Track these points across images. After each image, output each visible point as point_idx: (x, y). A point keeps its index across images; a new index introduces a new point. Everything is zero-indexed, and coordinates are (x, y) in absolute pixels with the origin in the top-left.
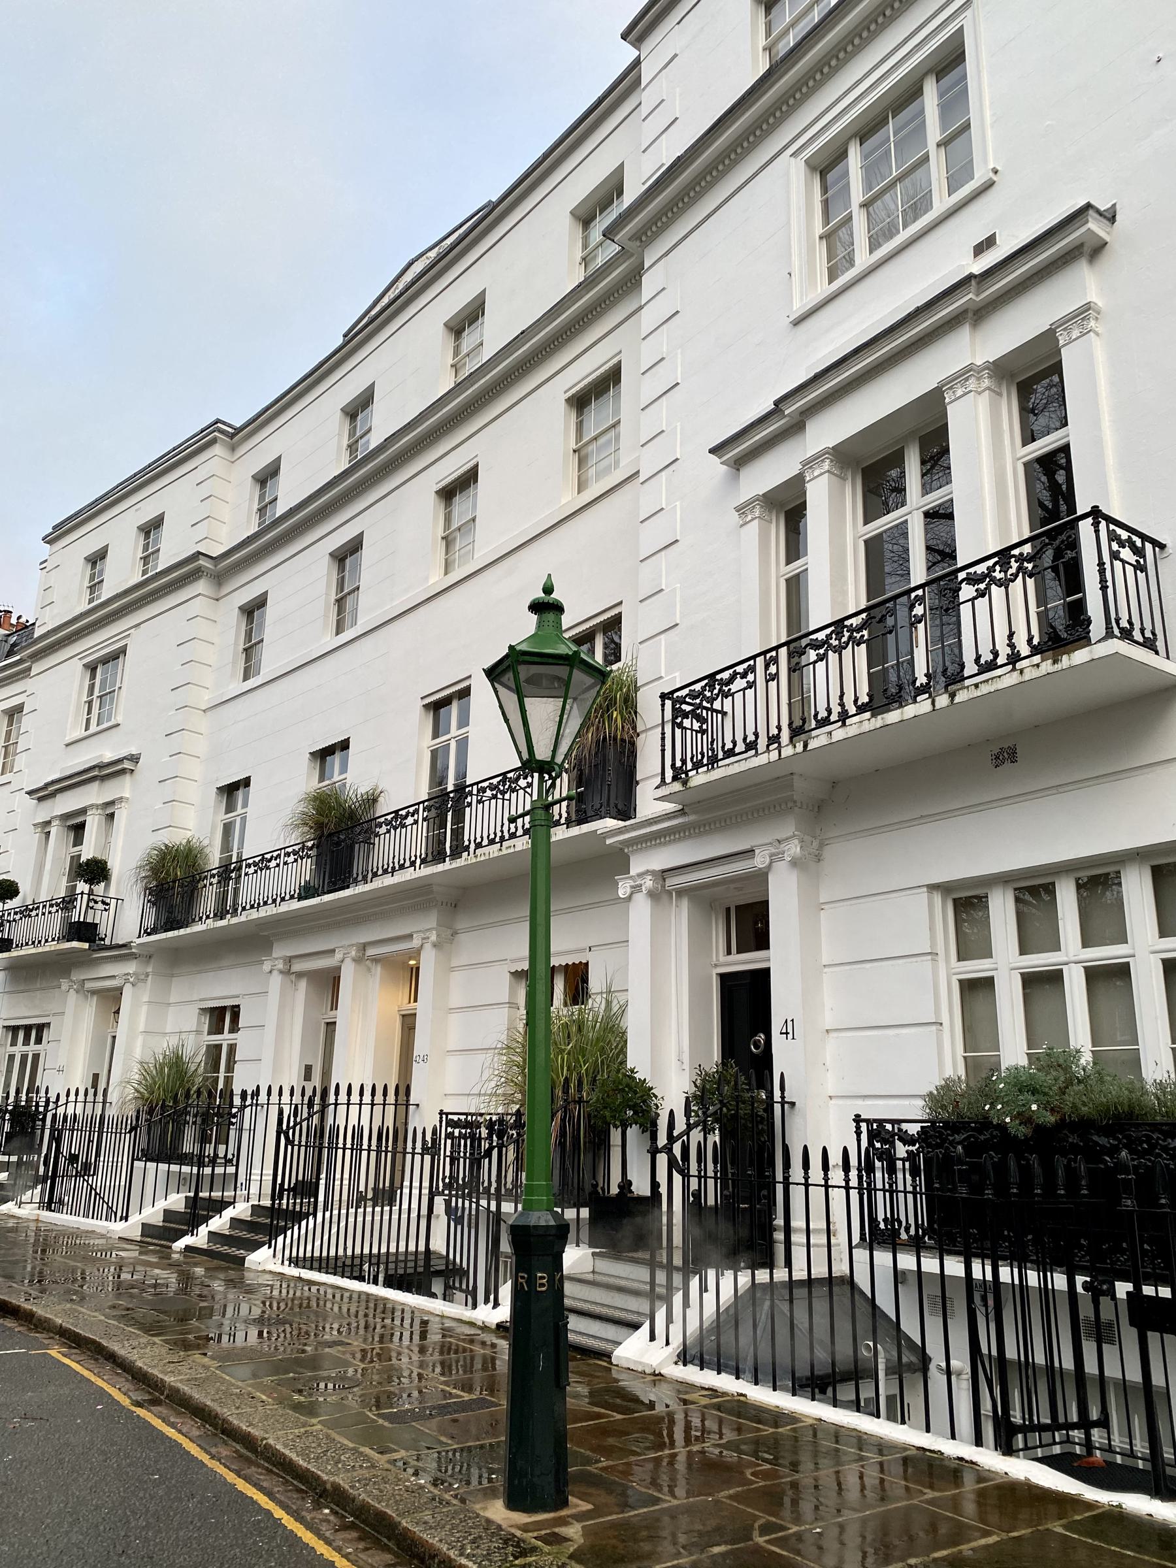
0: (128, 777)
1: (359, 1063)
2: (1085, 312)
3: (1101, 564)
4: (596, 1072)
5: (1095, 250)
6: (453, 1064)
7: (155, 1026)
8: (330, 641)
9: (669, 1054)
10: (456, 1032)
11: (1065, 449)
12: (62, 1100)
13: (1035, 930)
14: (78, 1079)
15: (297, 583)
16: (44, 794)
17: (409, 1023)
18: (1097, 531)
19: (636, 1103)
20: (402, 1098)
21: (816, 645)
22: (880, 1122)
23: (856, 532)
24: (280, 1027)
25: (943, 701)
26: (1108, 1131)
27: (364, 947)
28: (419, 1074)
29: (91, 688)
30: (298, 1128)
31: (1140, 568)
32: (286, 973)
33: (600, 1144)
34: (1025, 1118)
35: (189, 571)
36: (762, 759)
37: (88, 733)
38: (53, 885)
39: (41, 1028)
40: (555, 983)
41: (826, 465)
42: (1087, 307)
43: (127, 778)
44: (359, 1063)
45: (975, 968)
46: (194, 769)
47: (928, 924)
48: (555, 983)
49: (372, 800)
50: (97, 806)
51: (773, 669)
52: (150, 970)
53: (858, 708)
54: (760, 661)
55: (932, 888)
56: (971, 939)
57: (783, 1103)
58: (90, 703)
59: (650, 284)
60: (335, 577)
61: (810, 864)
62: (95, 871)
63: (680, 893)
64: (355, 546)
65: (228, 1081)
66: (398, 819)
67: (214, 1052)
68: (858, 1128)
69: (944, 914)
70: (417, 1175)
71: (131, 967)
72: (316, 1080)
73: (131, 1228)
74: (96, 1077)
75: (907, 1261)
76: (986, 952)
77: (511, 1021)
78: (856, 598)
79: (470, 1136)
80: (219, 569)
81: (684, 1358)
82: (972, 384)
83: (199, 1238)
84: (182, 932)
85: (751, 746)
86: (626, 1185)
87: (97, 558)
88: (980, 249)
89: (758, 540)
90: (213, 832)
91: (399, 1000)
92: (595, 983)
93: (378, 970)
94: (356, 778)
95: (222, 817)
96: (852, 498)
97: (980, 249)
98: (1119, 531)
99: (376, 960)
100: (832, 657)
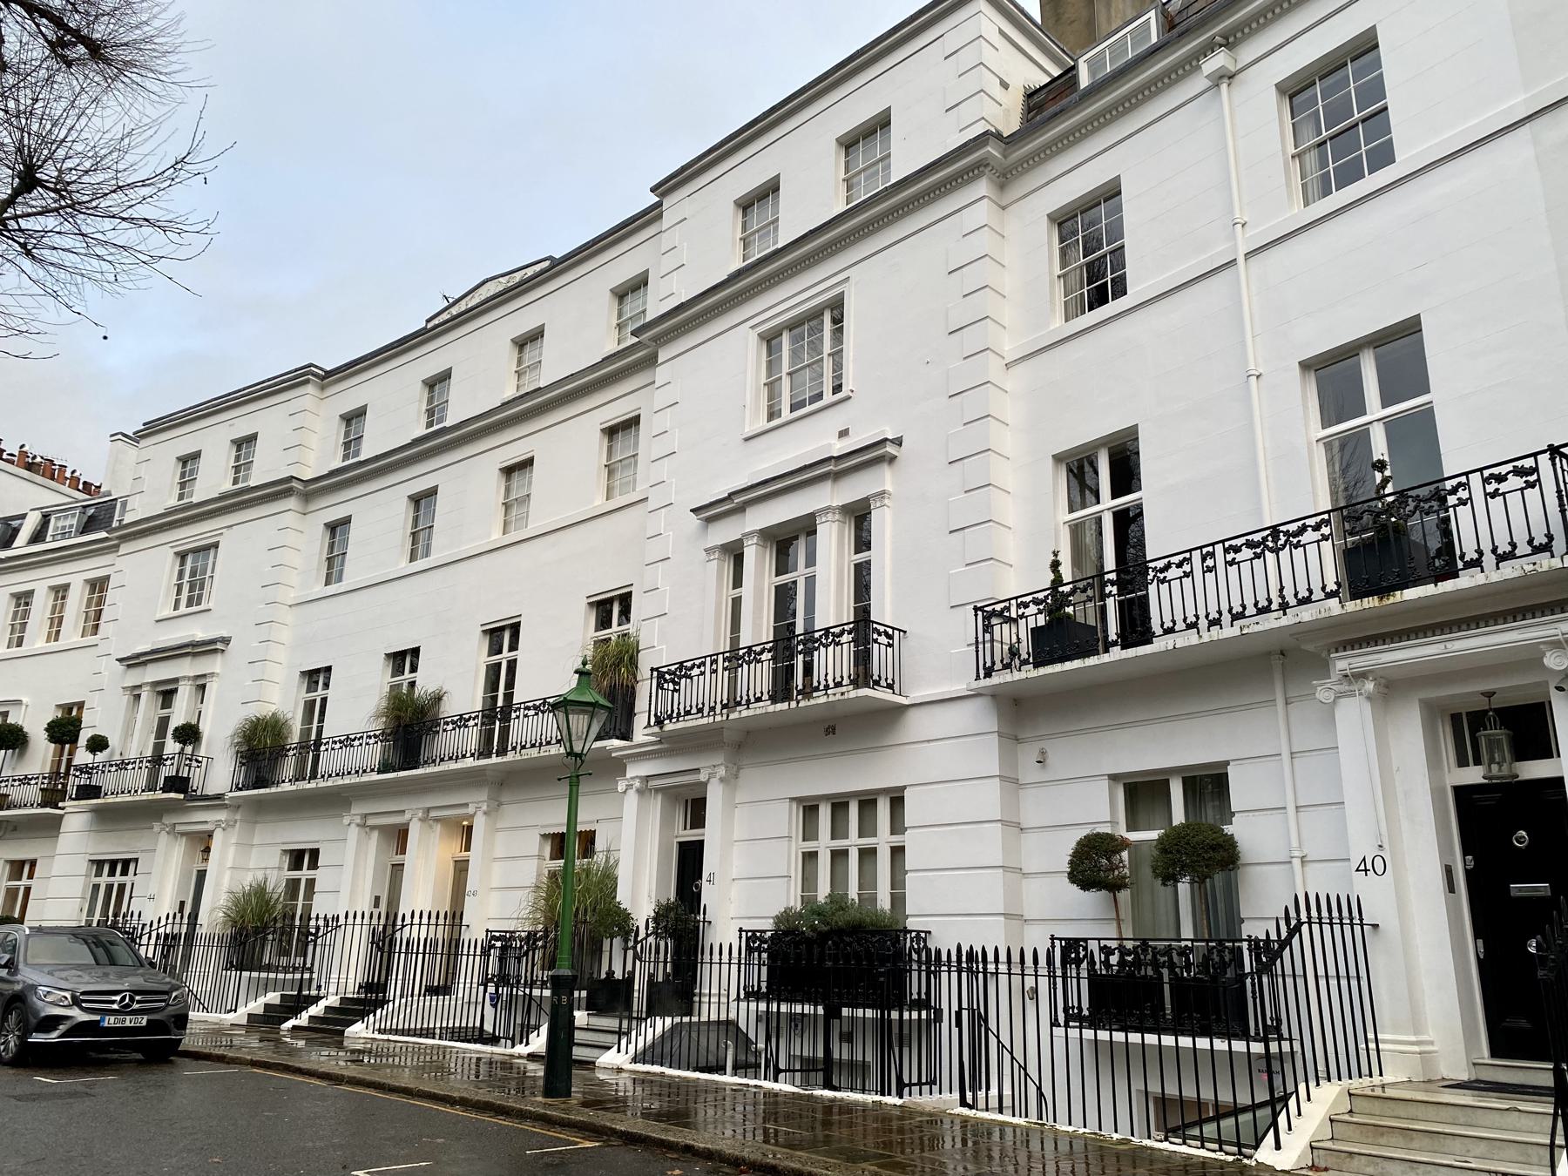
0: (219, 656)
1: (422, 893)
4: (597, 902)
6: (495, 897)
7: (242, 863)
8: (404, 566)
9: (641, 891)
10: (498, 874)
12: (163, 922)
13: (838, 831)
14: (167, 906)
15: (379, 515)
16: (134, 662)
17: (461, 868)
18: (1554, 465)
19: (620, 923)
20: (457, 921)
22: (754, 932)
23: (771, 581)
24: (356, 865)
25: (793, 704)
26: (850, 934)
27: (428, 810)
28: (469, 902)
29: (181, 574)
32: (363, 826)
33: (597, 951)
34: (813, 928)
35: (281, 489)
36: (705, 721)
37: (176, 613)
38: (140, 745)
39: (126, 863)
40: (570, 844)
42: (884, 492)
44: (422, 893)
45: (810, 846)
46: (280, 654)
47: (787, 819)
48: (570, 844)
49: (438, 699)
50: (189, 678)
51: (1210, 562)
52: (238, 817)
55: (792, 799)
56: (810, 832)
58: (180, 587)
59: (661, 374)
60: (411, 515)
62: (189, 734)
63: (657, 790)
65: (308, 909)
66: (461, 721)
67: (293, 885)
69: (797, 816)
70: (469, 969)
71: (222, 815)
72: (383, 908)
73: (240, 1016)
74: (182, 904)
77: (539, 868)
78: (767, 634)
79: (504, 946)
80: (311, 491)
81: (635, 1060)
82: (830, 516)
83: (303, 1019)
85: (700, 711)
86: (610, 973)
87: (189, 460)
88: (843, 434)
89: (716, 572)
91: (453, 849)
92: (600, 845)
93: (438, 827)
94: (426, 680)
95: (305, 696)
96: (770, 562)
97: (843, 434)
99: (437, 820)
100: (1270, 556)
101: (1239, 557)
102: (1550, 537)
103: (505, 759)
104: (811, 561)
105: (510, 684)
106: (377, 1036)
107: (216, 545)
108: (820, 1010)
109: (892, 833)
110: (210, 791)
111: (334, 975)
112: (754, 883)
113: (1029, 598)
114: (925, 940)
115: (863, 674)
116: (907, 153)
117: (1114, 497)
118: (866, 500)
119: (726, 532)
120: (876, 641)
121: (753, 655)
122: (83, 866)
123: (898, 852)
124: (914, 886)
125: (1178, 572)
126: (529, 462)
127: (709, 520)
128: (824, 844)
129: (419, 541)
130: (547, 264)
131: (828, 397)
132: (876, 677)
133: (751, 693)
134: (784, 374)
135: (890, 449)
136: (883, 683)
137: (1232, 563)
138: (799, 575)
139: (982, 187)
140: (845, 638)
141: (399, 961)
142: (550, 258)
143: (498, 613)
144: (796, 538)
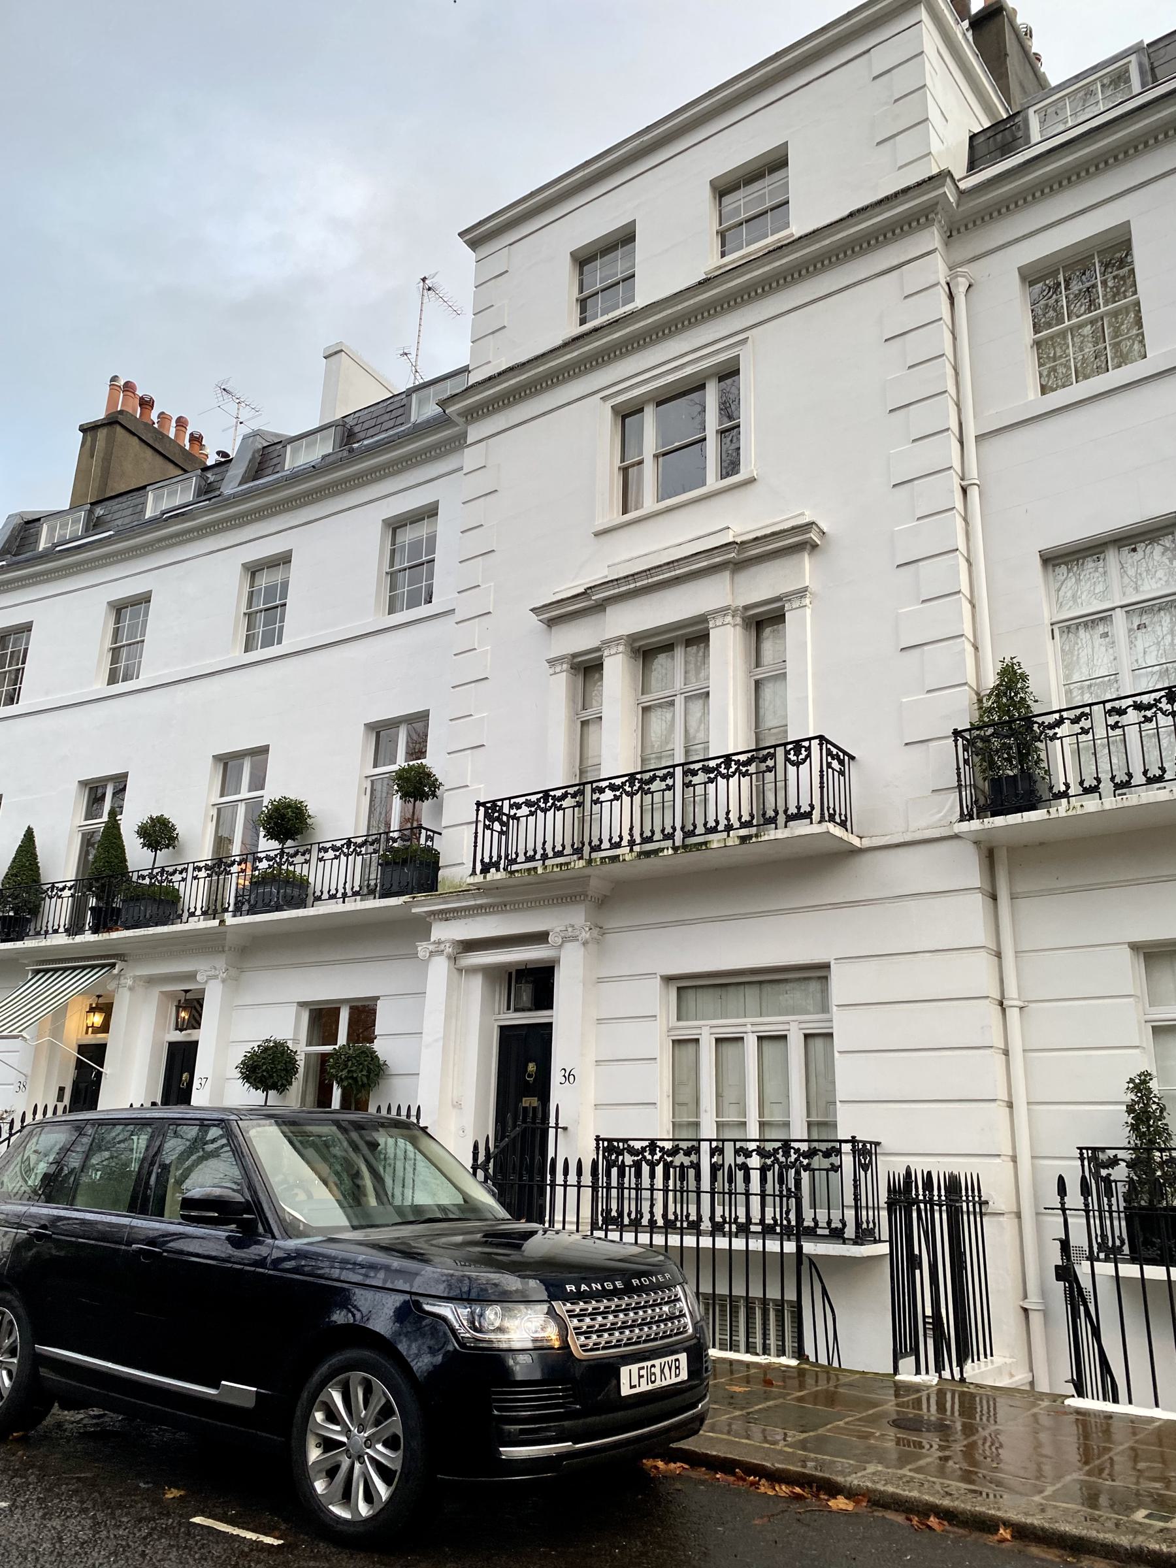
3: (821, 771)
21: (707, 770)
31: (842, 773)
41: (565, 666)
42: (805, 589)
47: (658, 1002)
53: (741, 823)
54: (506, 803)
57: (557, 1127)
59: (470, 457)
60: (111, 625)
61: (233, 982)
68: (1081, 1154)
75: (1130, 1270)
82: (729, 619)
84: (19, 945)
98: (832, 749)
101: (520, 813)
102: (812, 806)
103: (79, 939)
109: (679, 1019)
113: (329, 845)
116: (815, 201)
118: (703, 619)
119: (578, 638)
124: (849, 1077)
125: (663, 785)
129: (121, 663)
131: (713, 481)
135: (814, 536)
137: (321, 859)
139: (932, 238)
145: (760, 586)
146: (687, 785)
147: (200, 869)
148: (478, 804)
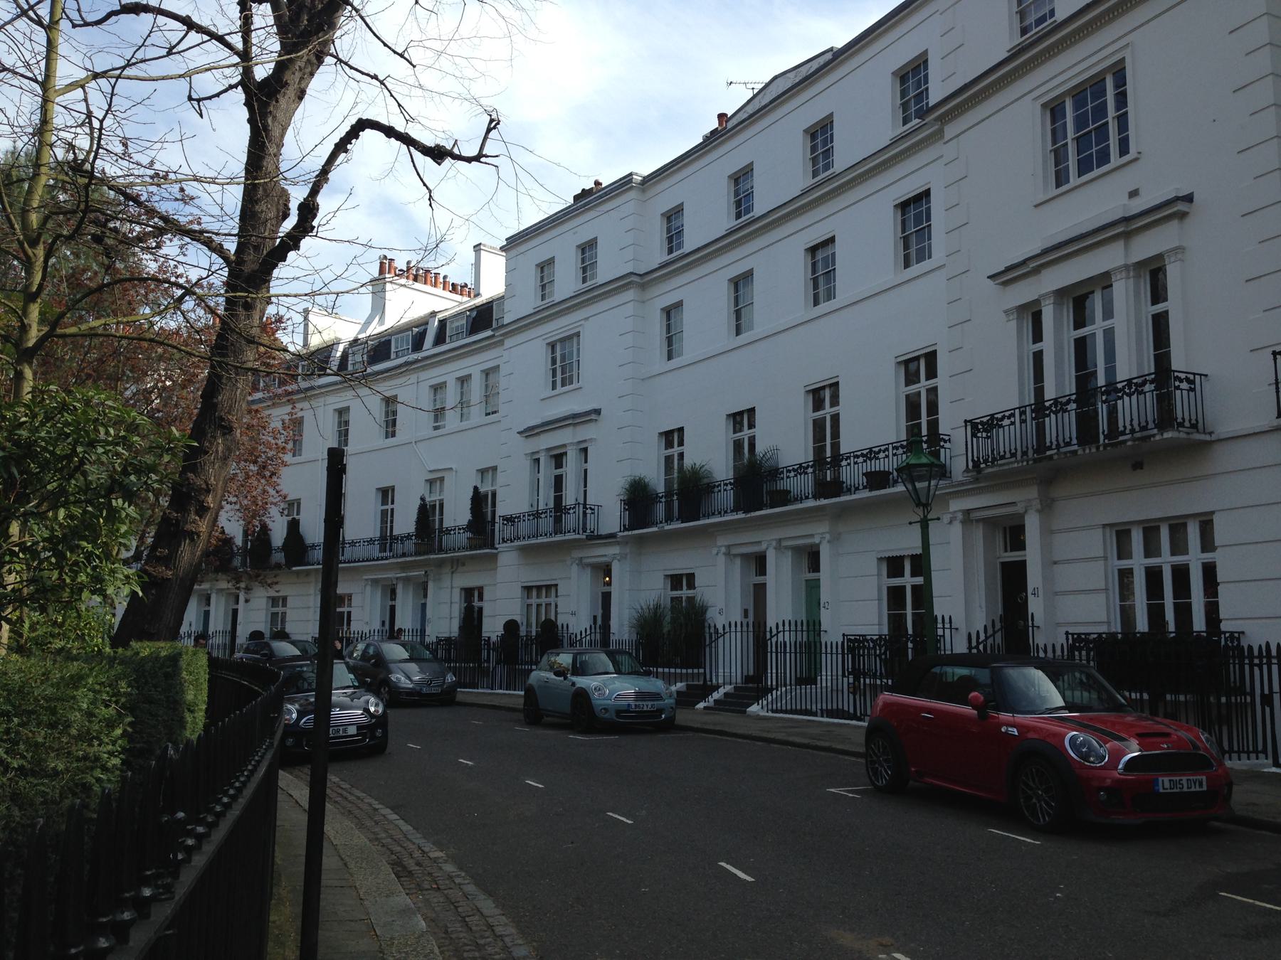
2: (1179, 250)
5: (1182, 216)
7: (639, 588)
11: (1167, 312)
13: (1151, 549)
16: (530, 432)
22: (1079, 635)
27: (780, 540)
30: (721, 640)
39: (548, 587)
43: (592, 425)
45: (1125, 564)
47: (1096, 543)
55: (1104, 526)
56: (1124, 553)
58: (554, 371)
64: (748, 276)
74: (595, 617)
76: (1129, 556)
78: (1070, 387)
79: (855, 645)
80: (641, 281)
84: (883, 492)
88: (1134, 194)
90: (67, 77)
100: (1126, 399)
104: (1108, 314)
105: (836, 434)
106: (770, 714)
107: (578, 334)
108: (1146, 696)
109: (1119, 558)
110: (603, 531)
111: (721, 670)
112: (1077, 591)
114: (1238, 639)
115: (1166, 417)
117: (927, 379)
118: (1160, 257)
119: (1024, 292)
120: (1178, 388)
121: (1059, 405)
122: (518, 592)
123: (1210, 571)
126: (832, 240)
127: (1005, 284)
128: (1138, 562)
130: (829, 56)
131: (1115, 160)
132: (1180, 420)
133: (1061, 438)
134: (1110, 119)
136: (1187, 424)
138: (1097, 328)
140: (1148, 387)
141: (772, 659)
142: (831, 49)
143: (818, 376)
144: (1093, 292)
145: (1146, 246)
146: (894, 455)
147: (897, 448)
148: (966, 421)
